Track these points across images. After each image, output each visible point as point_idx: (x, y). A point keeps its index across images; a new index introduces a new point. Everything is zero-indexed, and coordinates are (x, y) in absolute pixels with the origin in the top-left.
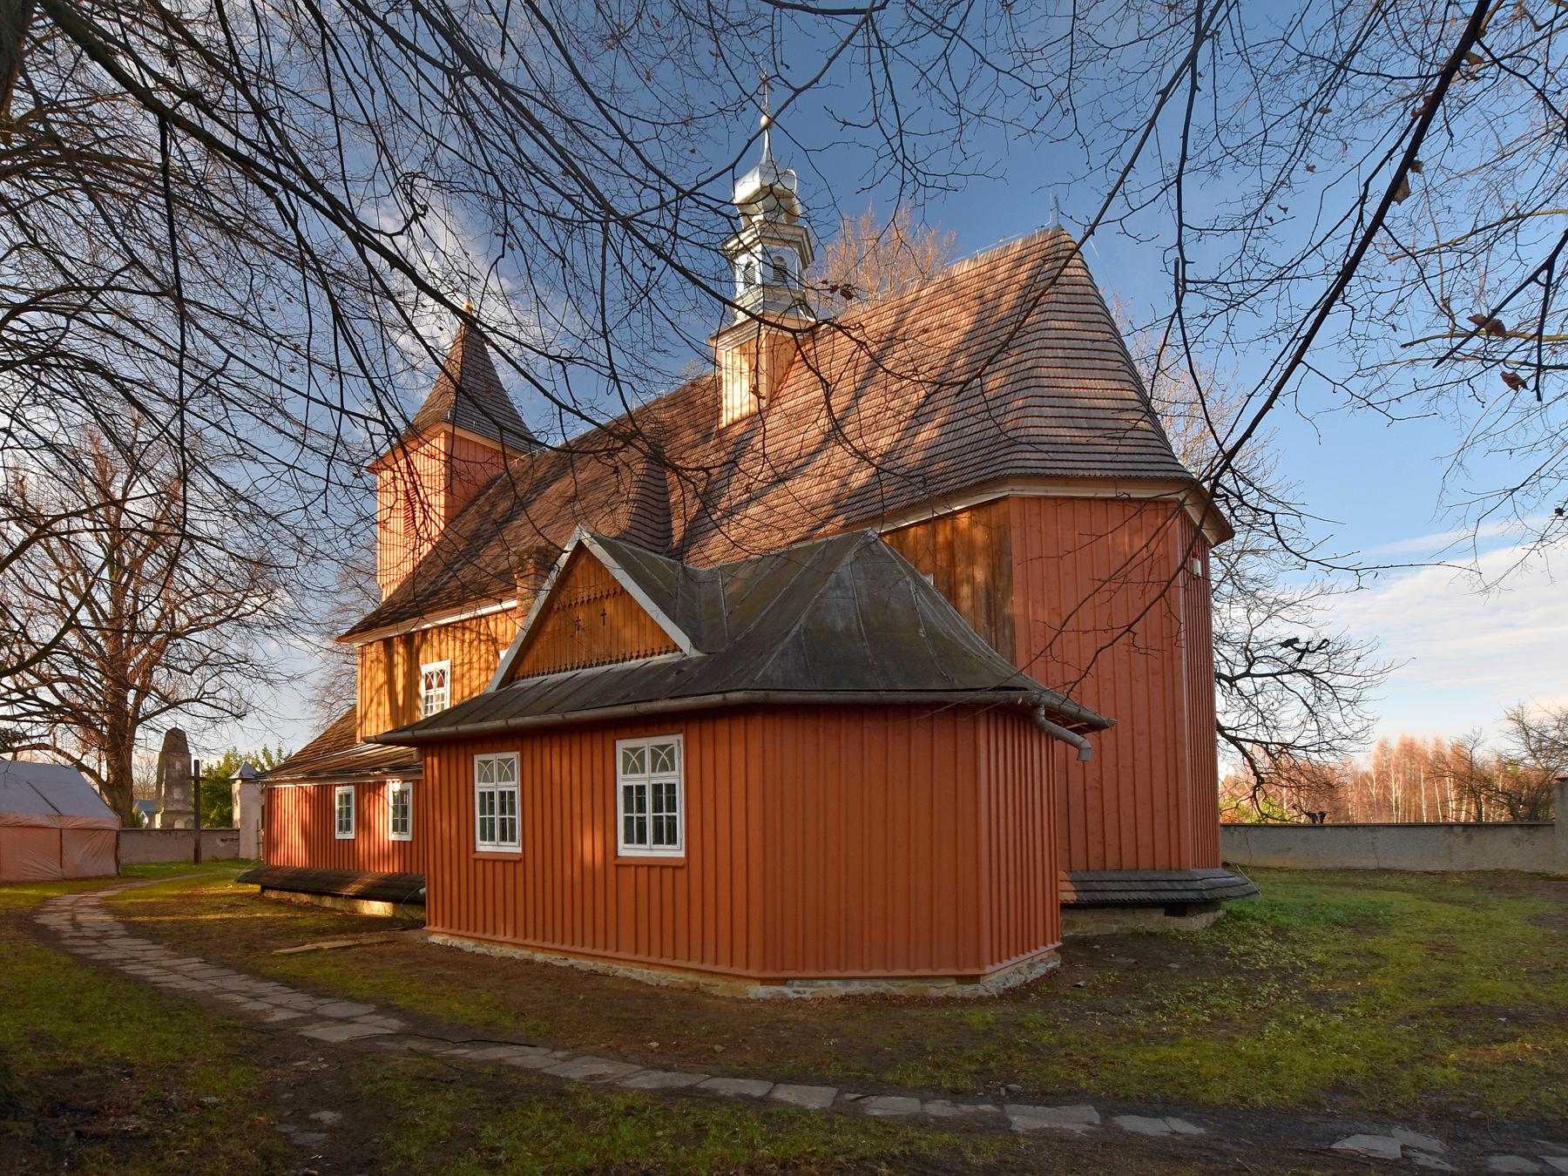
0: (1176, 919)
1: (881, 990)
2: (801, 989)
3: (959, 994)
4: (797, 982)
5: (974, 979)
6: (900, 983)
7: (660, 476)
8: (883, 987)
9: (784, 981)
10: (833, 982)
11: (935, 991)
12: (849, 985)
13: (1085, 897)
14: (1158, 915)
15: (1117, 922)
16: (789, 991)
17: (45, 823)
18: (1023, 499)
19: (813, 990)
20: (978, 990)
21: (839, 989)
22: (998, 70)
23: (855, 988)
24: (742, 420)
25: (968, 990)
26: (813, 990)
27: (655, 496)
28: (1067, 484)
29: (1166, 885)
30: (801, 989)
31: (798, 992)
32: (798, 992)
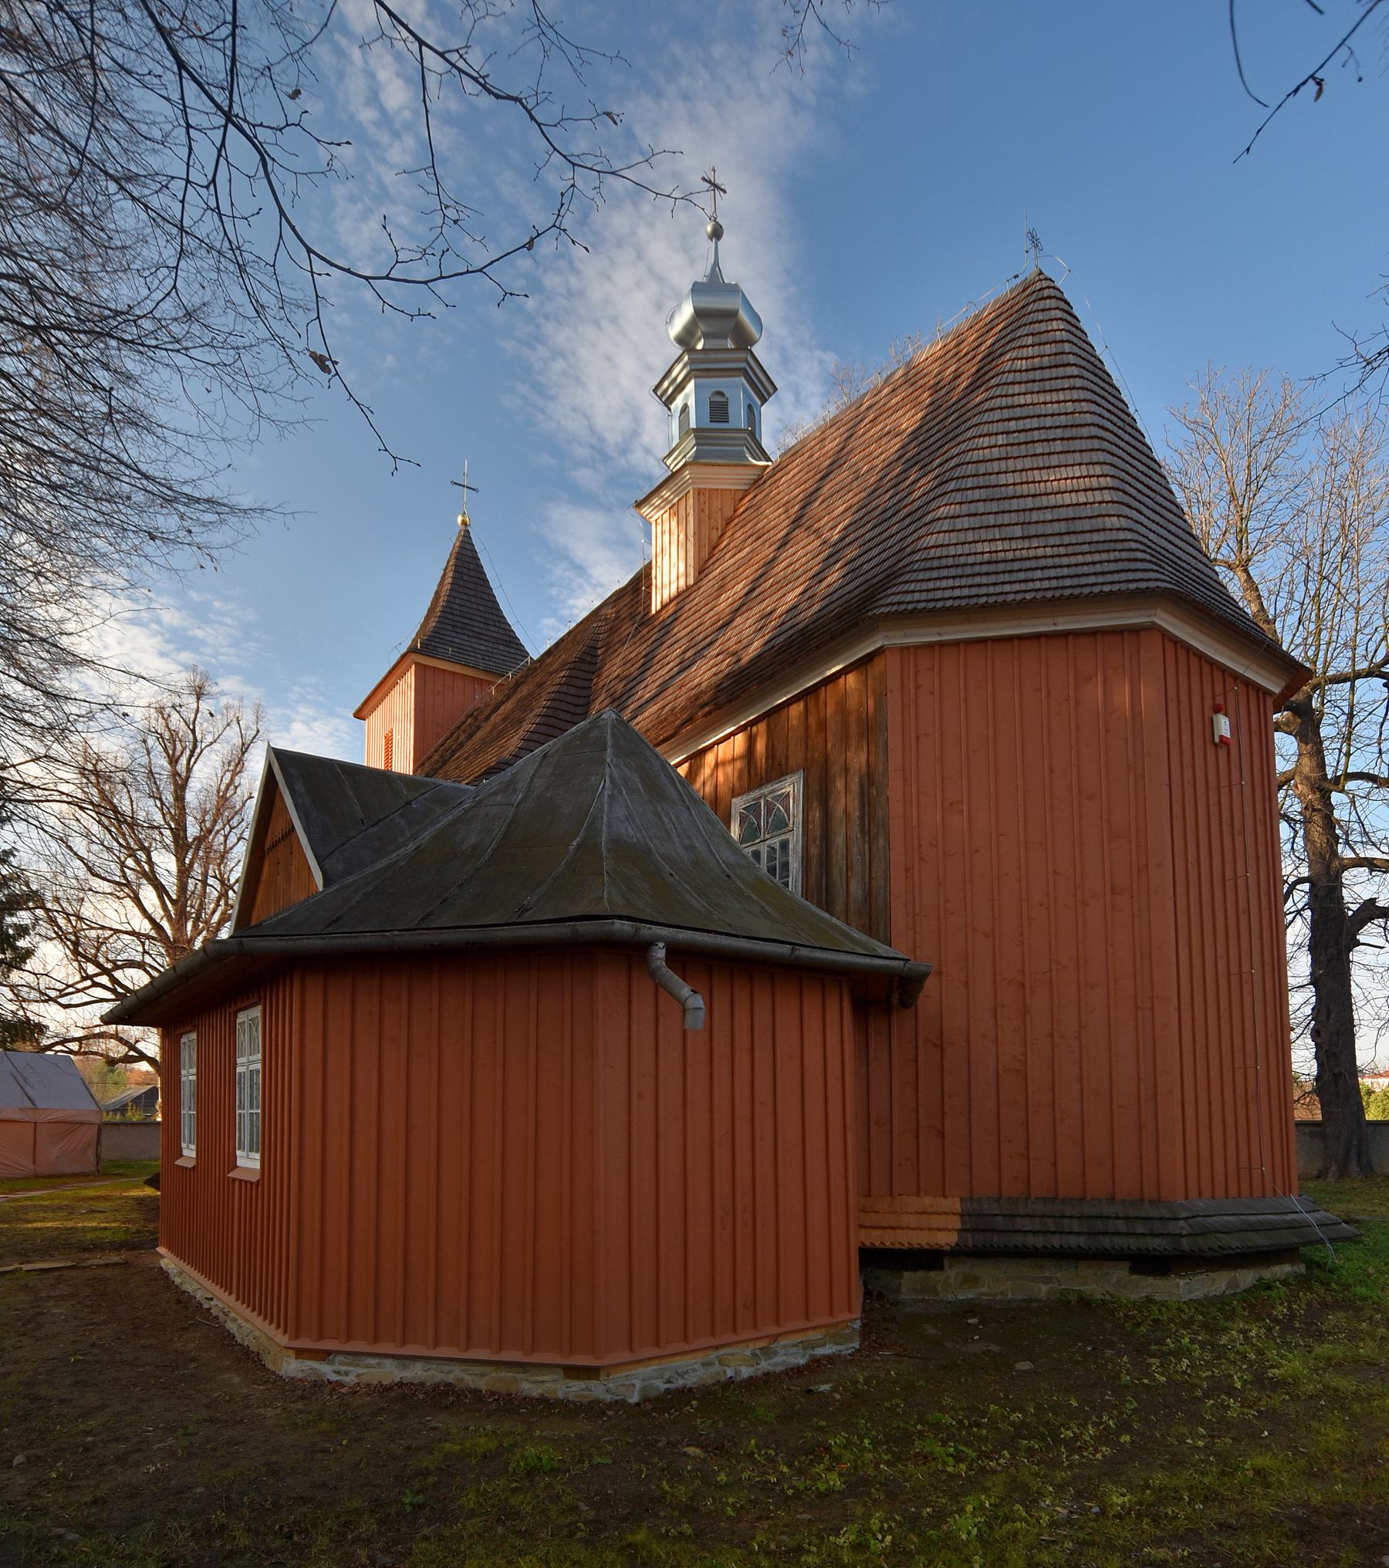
0: (1150, 1280)
1: (450, 1379)
2: (344, 1368)
3: (561, 1395)
4: (341, 1358)
5: (589, 1373)
6: (477, 1370)
7: (585, 684)
8: (455, 1375)
9: (324, 1355)
10: (388, 1362)
11: (530, 1386)
12: (405, 1367)
13: (970, 1240)
14: (1120, 1272)
15: (1049, 1280)
16: (326, 1370)
17: (17, 1117)
18: (904, 649)
19: (360, 1371)
20: (597, 1390)
21: (390, 1372)
22: (426, 283)
23: (416, 1373)
24: (671, 601)
25: (573, 1389)
26: (360, 1371)
27: (572, 709)
28: (968, 621)
29: (1121, 1226)
30: (344, 1368)
31: (338, 1373)
32: (338, 1373)
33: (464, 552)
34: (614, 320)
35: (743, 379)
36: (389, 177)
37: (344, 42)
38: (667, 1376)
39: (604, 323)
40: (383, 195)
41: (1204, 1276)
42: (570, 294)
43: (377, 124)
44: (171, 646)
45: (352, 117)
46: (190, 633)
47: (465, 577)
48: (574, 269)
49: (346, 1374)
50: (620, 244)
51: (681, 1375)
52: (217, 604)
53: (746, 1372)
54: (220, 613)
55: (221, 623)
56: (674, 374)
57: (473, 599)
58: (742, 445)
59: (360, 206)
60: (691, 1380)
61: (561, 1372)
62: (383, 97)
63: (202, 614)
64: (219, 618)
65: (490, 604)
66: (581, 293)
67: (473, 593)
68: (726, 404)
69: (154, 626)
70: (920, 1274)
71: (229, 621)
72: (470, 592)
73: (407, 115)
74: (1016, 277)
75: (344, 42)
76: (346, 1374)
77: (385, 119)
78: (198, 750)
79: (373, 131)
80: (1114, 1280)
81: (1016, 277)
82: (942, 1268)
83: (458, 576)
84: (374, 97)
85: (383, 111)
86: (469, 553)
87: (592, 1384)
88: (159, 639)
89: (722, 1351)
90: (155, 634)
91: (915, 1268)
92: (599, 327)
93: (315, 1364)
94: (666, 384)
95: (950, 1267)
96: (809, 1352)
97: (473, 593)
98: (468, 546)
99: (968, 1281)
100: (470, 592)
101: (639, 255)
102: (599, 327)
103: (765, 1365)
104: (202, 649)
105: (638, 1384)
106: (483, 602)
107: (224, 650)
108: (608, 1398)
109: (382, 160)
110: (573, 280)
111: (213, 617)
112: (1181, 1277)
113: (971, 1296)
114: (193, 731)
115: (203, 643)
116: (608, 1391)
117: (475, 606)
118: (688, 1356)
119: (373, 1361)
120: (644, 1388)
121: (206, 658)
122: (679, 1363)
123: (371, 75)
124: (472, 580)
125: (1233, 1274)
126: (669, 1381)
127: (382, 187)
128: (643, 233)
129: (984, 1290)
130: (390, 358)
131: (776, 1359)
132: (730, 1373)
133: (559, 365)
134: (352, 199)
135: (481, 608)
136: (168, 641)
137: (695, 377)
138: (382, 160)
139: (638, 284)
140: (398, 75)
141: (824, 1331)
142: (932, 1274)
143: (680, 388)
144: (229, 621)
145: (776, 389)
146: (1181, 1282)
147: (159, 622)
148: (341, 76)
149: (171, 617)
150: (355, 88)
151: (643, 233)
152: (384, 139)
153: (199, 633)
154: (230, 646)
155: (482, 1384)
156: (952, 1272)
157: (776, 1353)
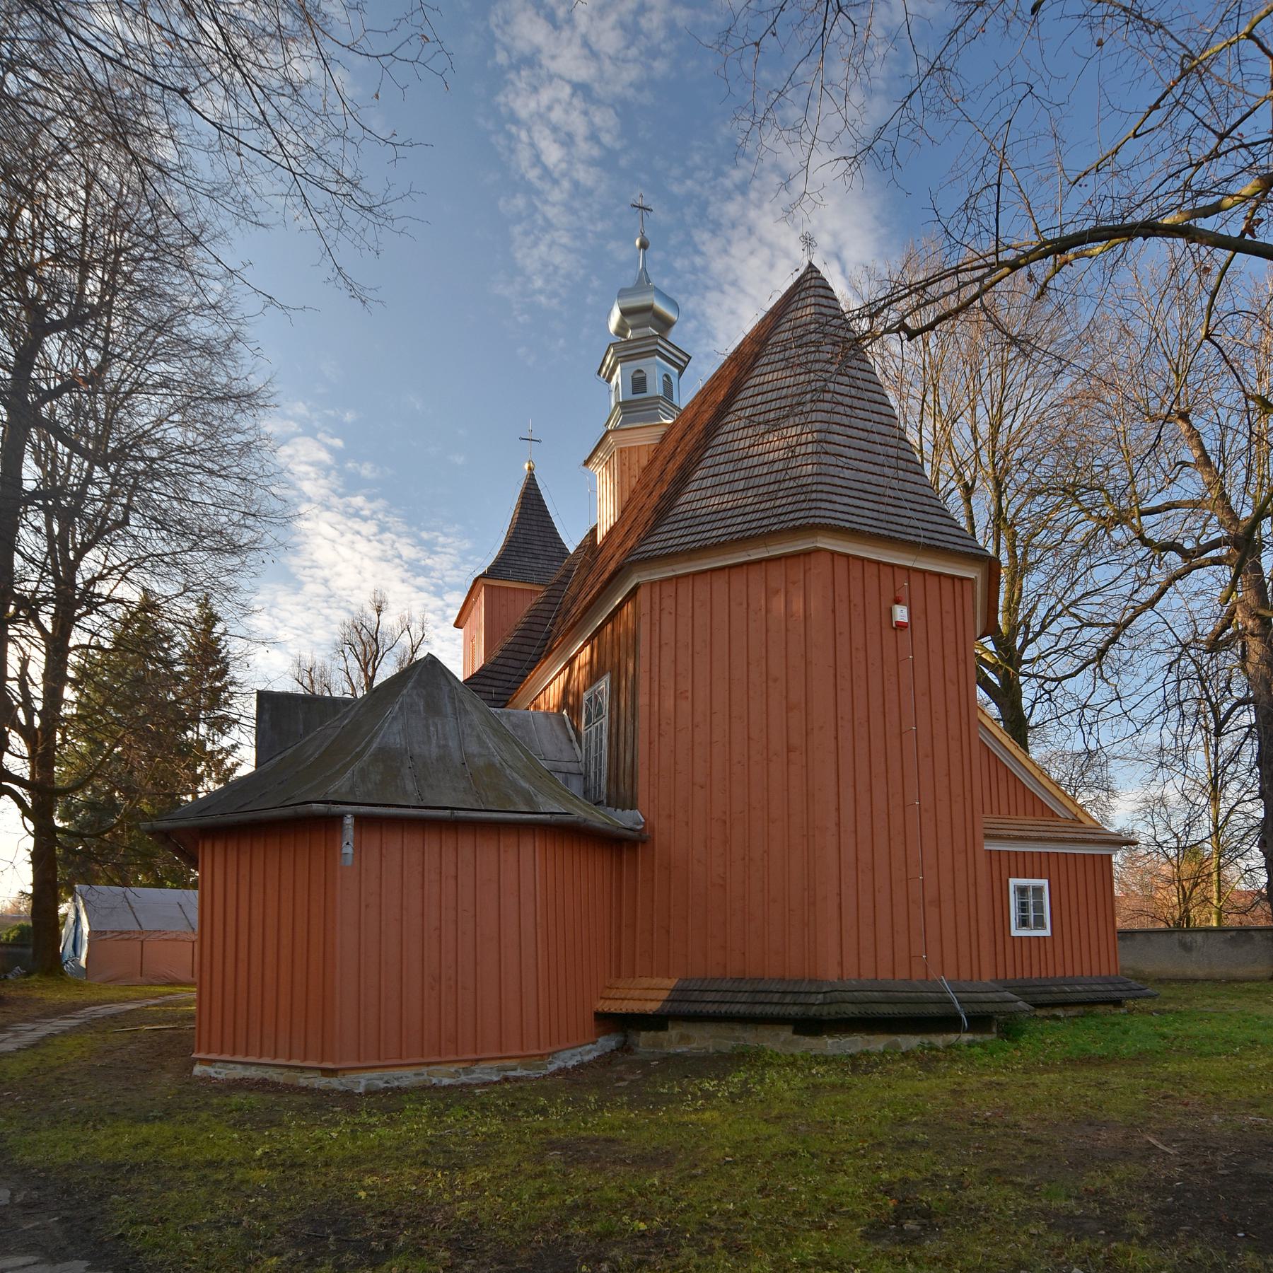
0: (807, 1039)
1: (266, 1076)
4: (219, 1064)
6: (279, 1071)
10: (239, 1066)
14: (786, 1033)
33: (529, 491)
34: (734, 283)
35: (657, 357)
36: (551, 212)
37: (514, 129)
38: (386, 1079)
39: (727, 288)
40: (549, 226)
41: (858, 1038)
42: (694, 270)
43: (541, 178)
44: (409, 574)
45: (523, 177)
46: (423, 563)
47: (529, 511)
48: (698, 252)
49: (220, 1073)
50: (734, 226)
51: (397, 1079)
52: (441, 539)
53: (446, 1081)
54: (444, 546)
55: (445, 553)
56: (608, 362)
57: (535, 528)
58: (657, 408)
59: (532, 237)
60: (404, 1083)
61: (320, 1072)
62: (544, 158)
63: (429, 547)
64: (444, 550)
65: (549, 530)
66: (705, 269)
67: (535, 523)
68: (644, 378)
69: (397, 561)
70: (652, 1033)
71: (452, 551)
72: (533, 523)
73: (564, 166)
74: (797, 270)
75: (514, 129)
76: (220, 1073)
77: (546, 173)
78: (380, 654)
79: (538, 184)
80: (782, 1039)
81: (797, 270)
82: (666, 1029)
83: (523, 511)
84: (537, 159)
85: (545, 168)
86: (533, 492)
87: (332, 1080)
88: (400, 569)
89: (432, 1068)
90: (397, 566)
91: (648, 1028)
92: (722, 292)
93: (206, 1068)
94: (604, 369)
95: (672, 1028)
96: (503, 1073)
97: (535, 523)
98: (532, 487)
99: (684, 1039)
100: (533, 523)
101: (750, 231)
102: (722, 292)
103: (463, 1078)
104: (432, 574)
105: (363, 1083)
106: (543, 529)
107: (448, 573)
108: (341, 1088)
109: (546, 202)
110: (698, 261)
111: (439, 549)
112: (830, 1036)
113: (685, 1050)
114: (376, 640)
115: (432, 569)
116: (341, 1084)
117: (536, 533)
118: (406, 1069)
119: (232, 1066)
120: (366, 1086)
121: (434, 580)
122: (398, 1072)
123: (532, 145)
124: (535, 513)
125: (893, 1038)
126: (386, 1082)
127: (546, 220)
128: (753, 214)
129: (694, 1045)
130: (562, 342)
131: (473, 1076)
132: (434, 1081)
133: (692, 325)
134: (526, 233)
135: (541, 534)
136: (407, 571)
137: (621, 362)
138: (546, 202)
139: (752, 253)
140: (555, 141)
141: (518, 1060)
142: (661, 1034)
143: (613, 371)
144: (452, 551)
145: (690, 358)
146: (830, 1041)
147: (400, 557)
148: (512, 151)
149: (408, 552)
150: (524, 156)
151: (753, 214)
152: (546, 186)
153: (429, 562)
154: (452, 569)
155: (281, 1079)
156: (674, 1032)
157: (473, 1072)
